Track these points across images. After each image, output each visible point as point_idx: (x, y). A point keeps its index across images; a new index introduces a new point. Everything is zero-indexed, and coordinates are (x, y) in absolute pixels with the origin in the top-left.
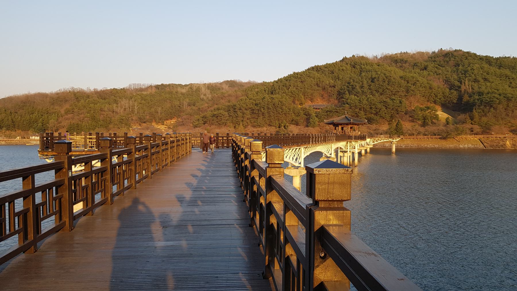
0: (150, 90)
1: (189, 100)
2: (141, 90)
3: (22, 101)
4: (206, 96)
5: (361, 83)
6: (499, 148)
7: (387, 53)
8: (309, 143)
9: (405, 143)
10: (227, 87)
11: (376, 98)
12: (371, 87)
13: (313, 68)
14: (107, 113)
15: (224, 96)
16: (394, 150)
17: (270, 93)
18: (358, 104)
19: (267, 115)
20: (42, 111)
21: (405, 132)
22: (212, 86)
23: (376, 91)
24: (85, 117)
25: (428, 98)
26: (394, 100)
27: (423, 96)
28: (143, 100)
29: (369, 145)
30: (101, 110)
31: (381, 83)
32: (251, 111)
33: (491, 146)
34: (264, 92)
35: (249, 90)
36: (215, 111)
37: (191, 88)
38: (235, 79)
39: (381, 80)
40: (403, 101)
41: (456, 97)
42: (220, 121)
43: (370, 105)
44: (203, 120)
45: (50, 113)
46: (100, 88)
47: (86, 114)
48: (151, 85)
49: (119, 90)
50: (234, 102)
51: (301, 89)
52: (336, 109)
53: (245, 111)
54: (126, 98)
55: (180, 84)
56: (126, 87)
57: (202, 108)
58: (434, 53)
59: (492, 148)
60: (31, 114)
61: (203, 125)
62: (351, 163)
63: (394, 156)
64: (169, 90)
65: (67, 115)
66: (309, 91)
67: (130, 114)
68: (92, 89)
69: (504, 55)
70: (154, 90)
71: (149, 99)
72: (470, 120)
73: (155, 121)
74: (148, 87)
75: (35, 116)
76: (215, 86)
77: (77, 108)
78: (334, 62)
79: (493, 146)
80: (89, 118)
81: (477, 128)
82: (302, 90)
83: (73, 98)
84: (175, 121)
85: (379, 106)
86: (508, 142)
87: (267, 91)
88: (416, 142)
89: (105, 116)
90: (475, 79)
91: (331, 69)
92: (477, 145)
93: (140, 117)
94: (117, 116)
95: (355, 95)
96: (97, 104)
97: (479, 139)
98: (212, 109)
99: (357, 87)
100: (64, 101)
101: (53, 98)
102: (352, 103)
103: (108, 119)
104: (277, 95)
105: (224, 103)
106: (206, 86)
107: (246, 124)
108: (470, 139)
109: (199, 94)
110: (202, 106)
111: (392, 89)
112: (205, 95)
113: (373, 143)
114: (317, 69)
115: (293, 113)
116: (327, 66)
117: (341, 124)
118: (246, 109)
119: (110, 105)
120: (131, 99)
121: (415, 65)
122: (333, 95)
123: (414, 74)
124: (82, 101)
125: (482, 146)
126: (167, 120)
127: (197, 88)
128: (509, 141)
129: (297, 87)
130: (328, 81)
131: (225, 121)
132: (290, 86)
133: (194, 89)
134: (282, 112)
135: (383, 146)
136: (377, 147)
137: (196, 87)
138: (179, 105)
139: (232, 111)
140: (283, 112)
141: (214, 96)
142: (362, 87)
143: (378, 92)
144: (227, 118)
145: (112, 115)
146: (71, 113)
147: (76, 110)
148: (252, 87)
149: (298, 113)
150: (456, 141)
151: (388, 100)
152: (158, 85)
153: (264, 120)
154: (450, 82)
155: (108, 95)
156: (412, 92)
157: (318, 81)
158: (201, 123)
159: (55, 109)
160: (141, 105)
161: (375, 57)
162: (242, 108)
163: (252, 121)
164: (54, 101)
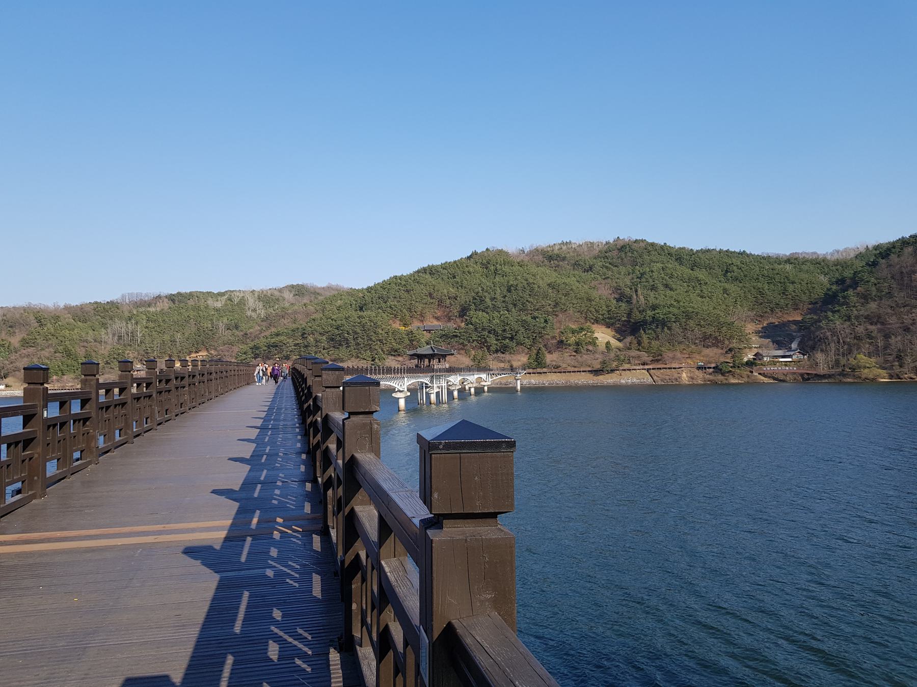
1: (228, 320)
4: (256, 313)
6: (672, 382)
7: (538, 245)
11: (513, 317)
13: (424, 270)
16: (519, 388)
17: (358, 309)
25: (586, 314)
27: (579, 312)
28: (150, 322)
29: (486, 382)
36: (272, 338)
37: (230, 300)
40: (549, 320)
49: (104, 304)
50: (302, 323)
54: (121, 318)
56: (116, 299)
57: (251, 333)
58: (607, 243)
59: (663, 383)
61: (254, 359)
64: (193, 303)
68: (62, 305)
70: (166, 305)
72: (637, 345)
74: (154, 298)
86: (684, 373)
91: (452, 271)
92: (644, 379)
98: (267, 333)
99: (487, 300)
104: (369, 311)
105: (286, 324)
110: (251, 330)
112: (254, 310)
113: (491, 378)
116: (445, 266)
120: (130, 320)
121: (576, 265)
123: (572, 280)
125: (650, 380)
127: (241, 299)
129: (400, 298)
130: (446, 289)
133: (236, 300)
136: (511, 385)
141: (270, 314)
148: (336, 295)
149: (401, 339)
151: (529, 318)
161: (521, 250)
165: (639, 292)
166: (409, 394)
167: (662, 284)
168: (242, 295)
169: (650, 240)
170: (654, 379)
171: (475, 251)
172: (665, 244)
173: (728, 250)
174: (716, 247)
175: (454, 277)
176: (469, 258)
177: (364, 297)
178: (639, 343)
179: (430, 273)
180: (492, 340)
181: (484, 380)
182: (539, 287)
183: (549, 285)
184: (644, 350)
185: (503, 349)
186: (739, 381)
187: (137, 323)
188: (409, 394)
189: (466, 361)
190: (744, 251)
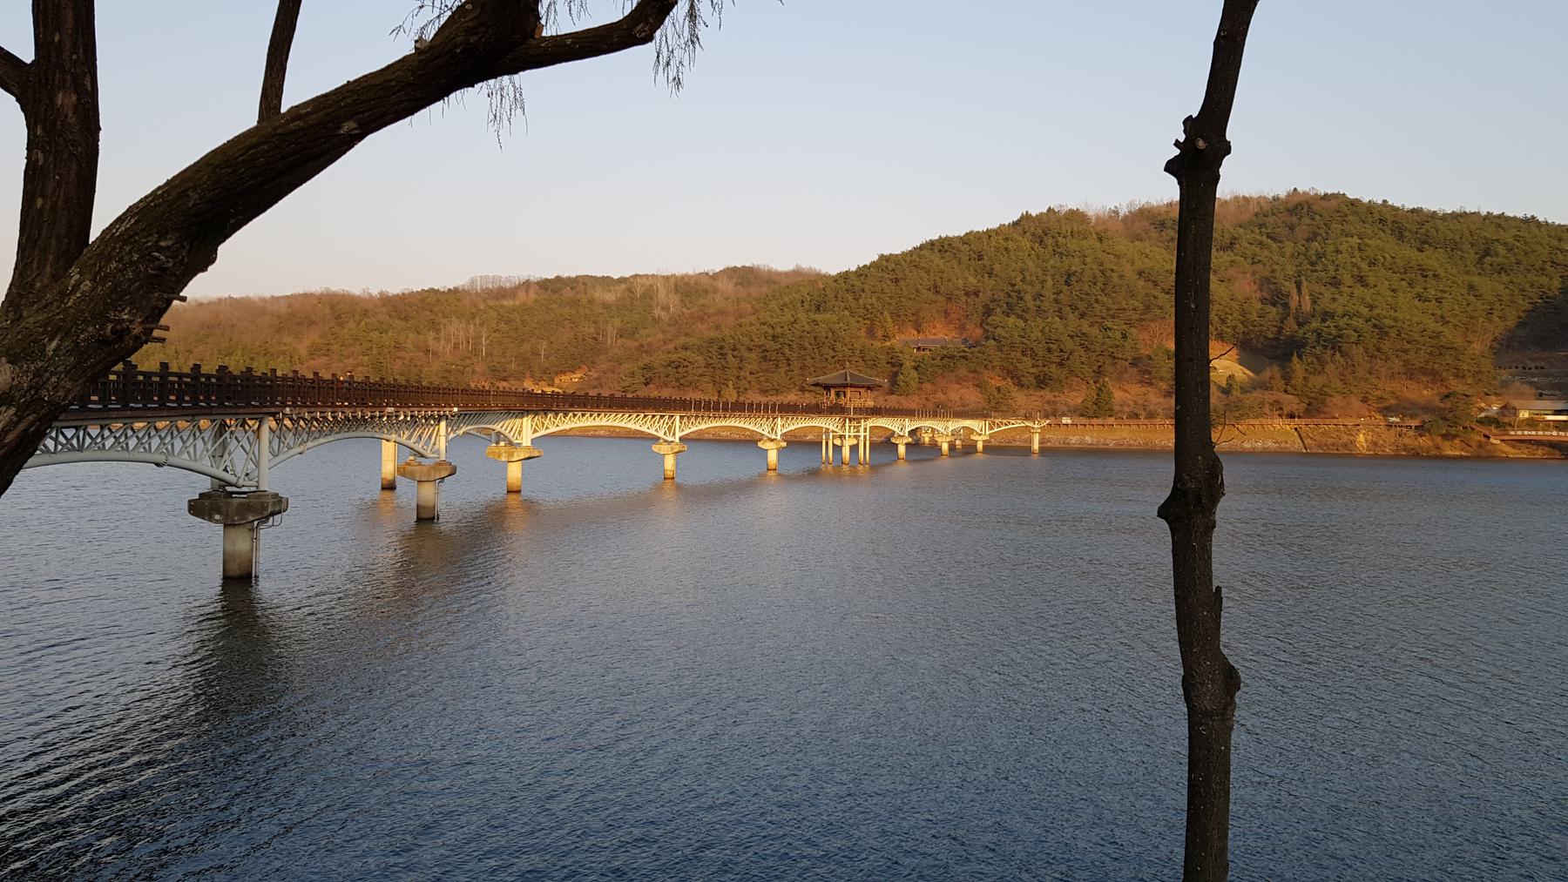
0: (524, 295)
1: (622, 321)
2: (501, 293)
3: (203, 323)
5: (1038, 286)
6: (1337, 450)
7: (1143, 202)
8: (690, 410)
9: (1117, 435)
10: (731, 286)
12: (1062, 296)
13: (931, 244)
14: (412, 354)
15: (706, 314)
16: (1036, 446)
18: (1017, 339)
19: (796, 364)
20: (252, 349)
21: (1117, 408)
22: (687, 284)
23: (1070, 306)
24: (358, 365)
26: (1110, 329)
29: (980, 435)
30: (398, 347)
31: (1086, 287)
32: (761, 355)
33: (1320, 446)
34: (800, 305)
35: (774, 297)
37: (630, 290)
38: (755, 264)
39: (1087, 279)
41: (1275, 323)
42: (685, 377)
43: (1047, 343)
44: (643, 376)
45: (272, 355)
46: (394, 289)
47: (361, 357)
48: (528, 280)
49: (444, 292)
51: (891, 298)
52: (964, 351)
53: (746, 354)
55: (605, 275)
57: (650, 345)
58: (1276, 199)
59: (1321, 451)
60: (226, 356)
62: (868, 459)
63: (1035, 457)
65: (314, 359)
66: (910, 304)
67: (469, 358)
68: (375, 292)
69: (1461, 207)
71: (518, 320)
73: (532, 376)
75: (235, 359)
76: (697, 284)
77: (337, 343)
78: (995, 226)
79: (1326, 445)
80: (368, 366)
81: (1291, 402)
82: (893, 302)
83: (328, 317)
84: (579, 376)
85: (1069, 345)
86: (1361, 435)
87: (806, 305)
88: (1142, 435)
89: (405, 361)
90: (1335, 278)
93: (494, 366)
94: (437, 363)
95: (1020, 317)
96: (387, 332)
97: (1296, 429)
99: (1028, 297)
100: (306, 325)
101: (279, 317)
102: (1003, 337)
103: (414, 370)
105: (704, 331)
106: (672, 282)
107: (747, 386)
108: (1272, 429)
109: (650, 306)
111: (1110, 302)
112: (666, 308)
114: (943, 246)
115: (860, 360)
116: (970, 239)
117: (834, 387)
118: (750, 350)
119: (419, 333)
122: (972, 314)
124: (351, 324)
125: (1298, 445)
126: (564, 373)
127: (647, 290)
128: (1364, 434)
131: (696, 378)
132: (863, 290)
133: (639, 291)
134: (833, 357)
135: (1064, 443)
136: (1049, 444)
137: (642, 286)
138: (595, 336)
139: (714, 352)
140: (836, 358)
142: (1039, 296)
143: (1077, 308)
144: (700, 371)
145: (424, 359)
146: (324, 355)
147: (336, 347)
150: (1237, 433)
151: (1095, 331)
152: (546, 279)
153: (788, 378)
154: (1274, 283)
155: (415, 308)
156: (1158, 312)
157: (938, 279)
158: (638, 381)
159: (285, 344)
160: (496, 335)
161: (1114, 212)
162: (739, 346)
163: (761, 379)
164: (281, 323)
165: (1304, 290)
166: (784, 444)
167: (1352, 276)
168: (651, 282)
169: (1351, 196)
170: (1306, 443)
171: (1027, 212)
172: (1385, 201)
173: (1503, 213)
174: (1479, 208)
175: (980, 258)
176: (1015, 224)
177: (824, 290)
178: (1287, 378)
179: (940, 251)
180: (1026, 366)
181: (977, 433)
182: (1121, 277)
183: (1140, 274)
184: (1295, 392)
185: (1042, 382)
186: (1463, 453)
187: (482, 324)
188: (784, 444)
189: (973, 397)
190: (1533, 217)
